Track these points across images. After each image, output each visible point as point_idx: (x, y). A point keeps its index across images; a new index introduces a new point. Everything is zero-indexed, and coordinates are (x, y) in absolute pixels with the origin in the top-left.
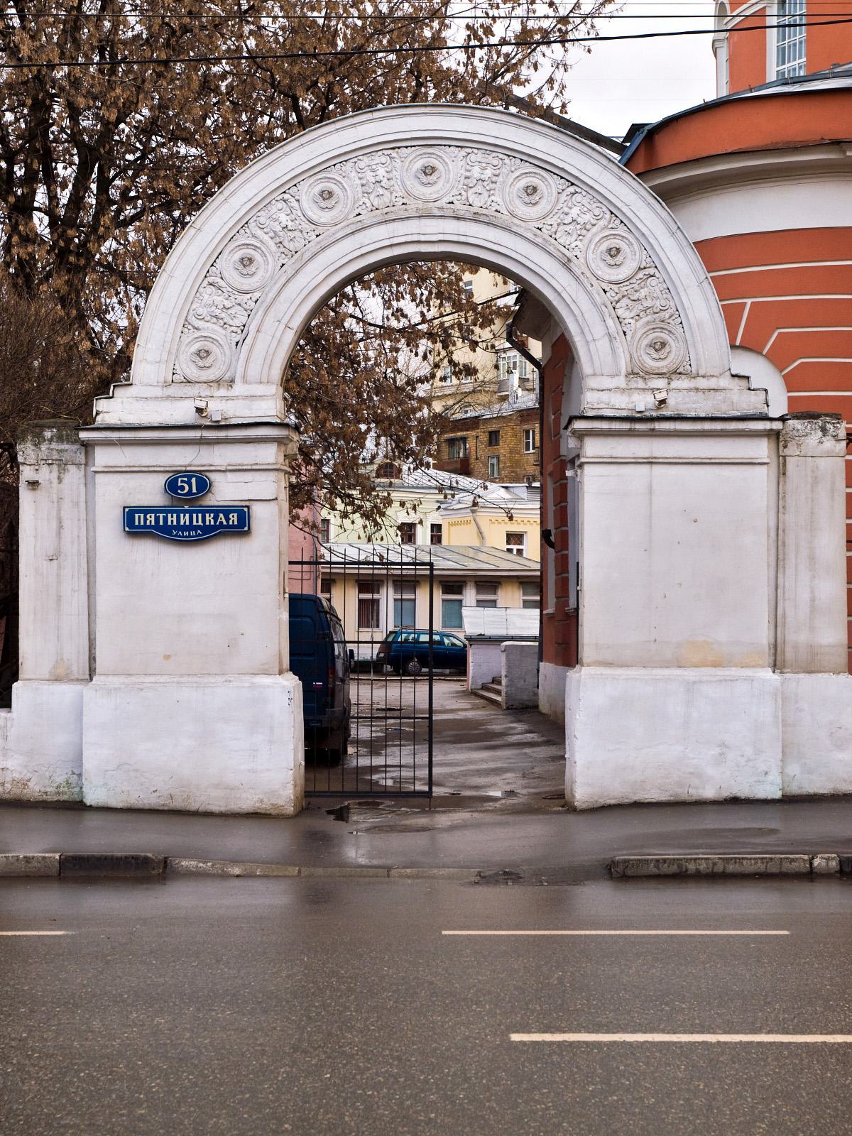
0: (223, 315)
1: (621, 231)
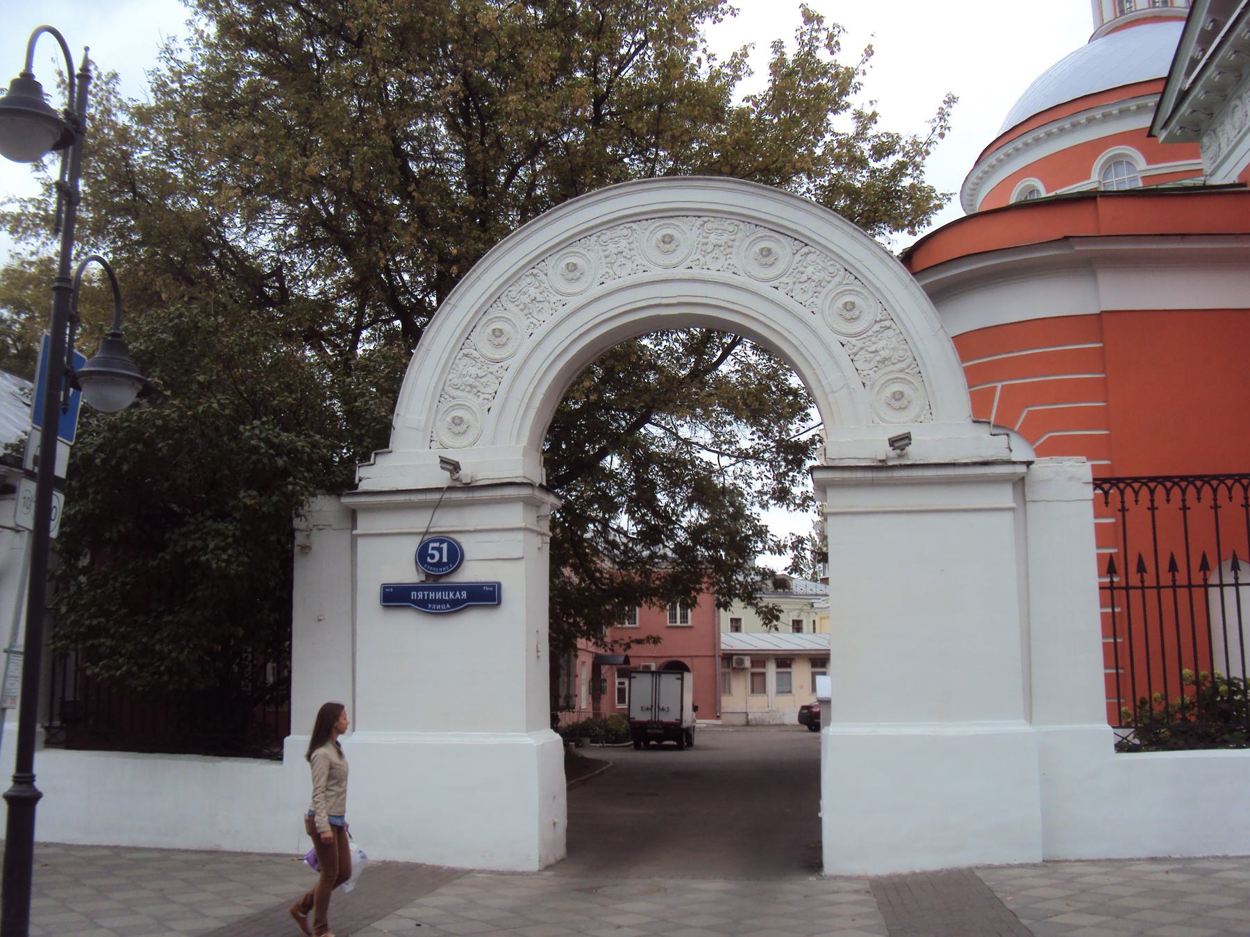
0: (477, 384)
1: (856, 286)
